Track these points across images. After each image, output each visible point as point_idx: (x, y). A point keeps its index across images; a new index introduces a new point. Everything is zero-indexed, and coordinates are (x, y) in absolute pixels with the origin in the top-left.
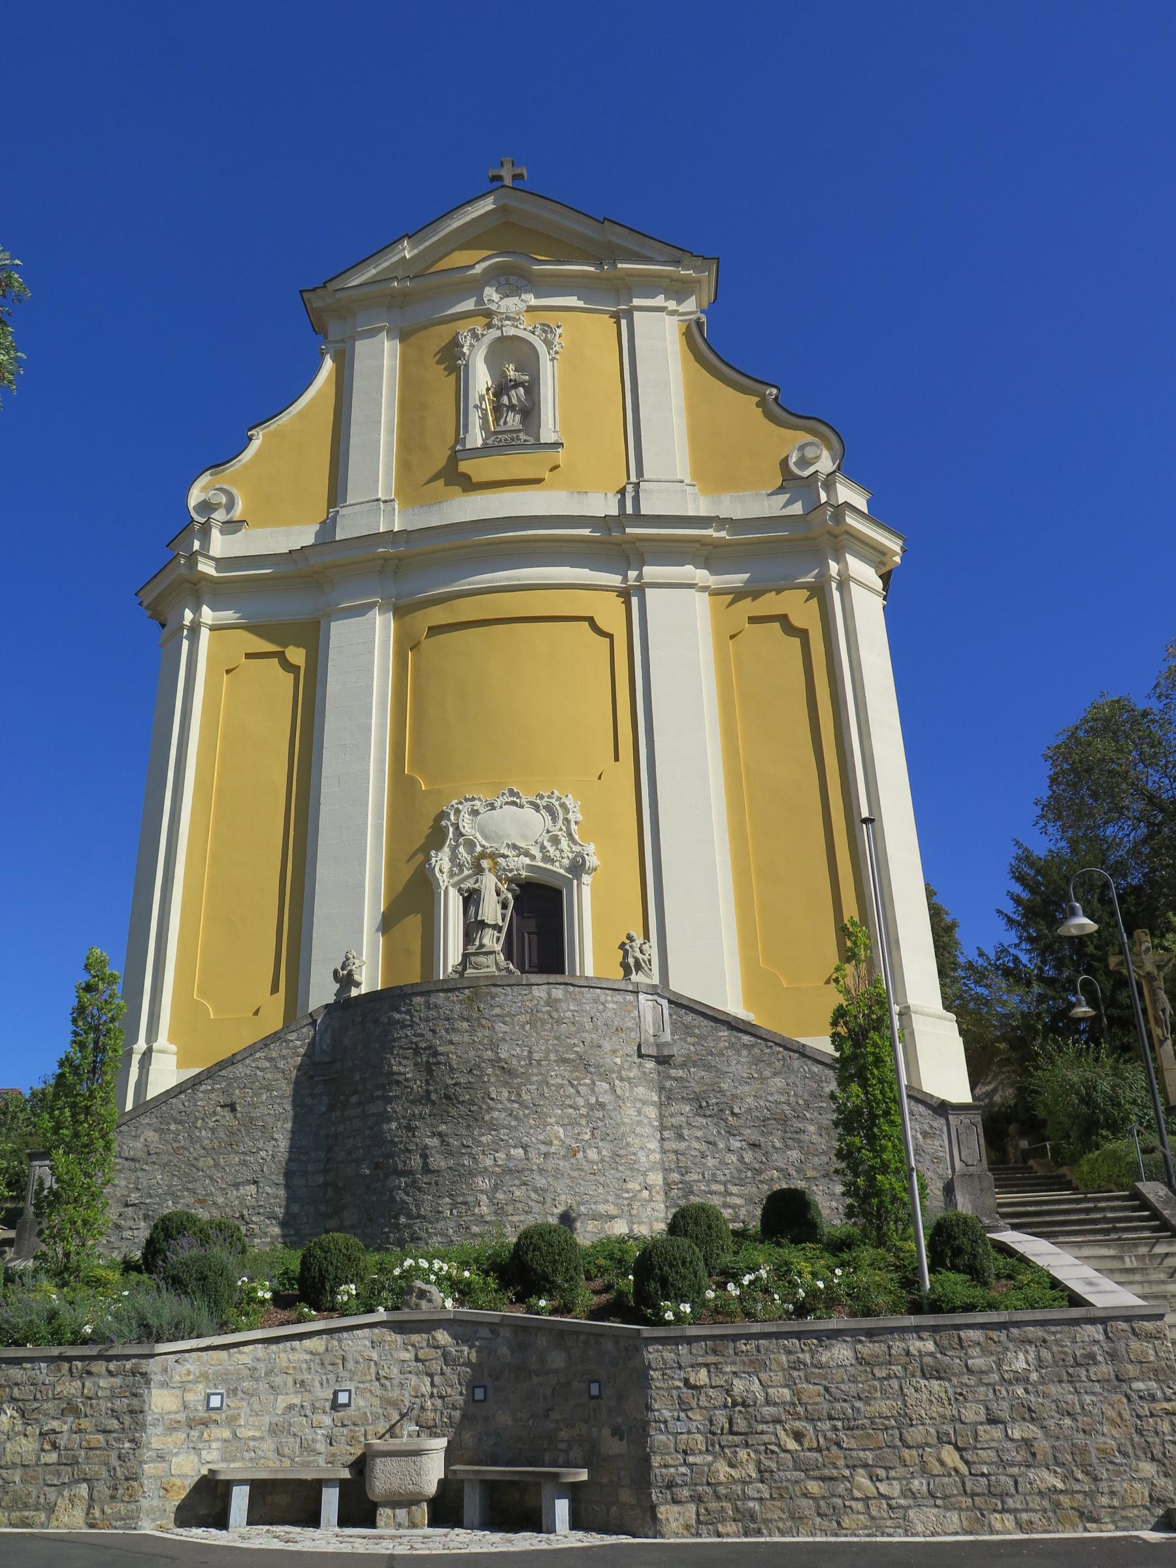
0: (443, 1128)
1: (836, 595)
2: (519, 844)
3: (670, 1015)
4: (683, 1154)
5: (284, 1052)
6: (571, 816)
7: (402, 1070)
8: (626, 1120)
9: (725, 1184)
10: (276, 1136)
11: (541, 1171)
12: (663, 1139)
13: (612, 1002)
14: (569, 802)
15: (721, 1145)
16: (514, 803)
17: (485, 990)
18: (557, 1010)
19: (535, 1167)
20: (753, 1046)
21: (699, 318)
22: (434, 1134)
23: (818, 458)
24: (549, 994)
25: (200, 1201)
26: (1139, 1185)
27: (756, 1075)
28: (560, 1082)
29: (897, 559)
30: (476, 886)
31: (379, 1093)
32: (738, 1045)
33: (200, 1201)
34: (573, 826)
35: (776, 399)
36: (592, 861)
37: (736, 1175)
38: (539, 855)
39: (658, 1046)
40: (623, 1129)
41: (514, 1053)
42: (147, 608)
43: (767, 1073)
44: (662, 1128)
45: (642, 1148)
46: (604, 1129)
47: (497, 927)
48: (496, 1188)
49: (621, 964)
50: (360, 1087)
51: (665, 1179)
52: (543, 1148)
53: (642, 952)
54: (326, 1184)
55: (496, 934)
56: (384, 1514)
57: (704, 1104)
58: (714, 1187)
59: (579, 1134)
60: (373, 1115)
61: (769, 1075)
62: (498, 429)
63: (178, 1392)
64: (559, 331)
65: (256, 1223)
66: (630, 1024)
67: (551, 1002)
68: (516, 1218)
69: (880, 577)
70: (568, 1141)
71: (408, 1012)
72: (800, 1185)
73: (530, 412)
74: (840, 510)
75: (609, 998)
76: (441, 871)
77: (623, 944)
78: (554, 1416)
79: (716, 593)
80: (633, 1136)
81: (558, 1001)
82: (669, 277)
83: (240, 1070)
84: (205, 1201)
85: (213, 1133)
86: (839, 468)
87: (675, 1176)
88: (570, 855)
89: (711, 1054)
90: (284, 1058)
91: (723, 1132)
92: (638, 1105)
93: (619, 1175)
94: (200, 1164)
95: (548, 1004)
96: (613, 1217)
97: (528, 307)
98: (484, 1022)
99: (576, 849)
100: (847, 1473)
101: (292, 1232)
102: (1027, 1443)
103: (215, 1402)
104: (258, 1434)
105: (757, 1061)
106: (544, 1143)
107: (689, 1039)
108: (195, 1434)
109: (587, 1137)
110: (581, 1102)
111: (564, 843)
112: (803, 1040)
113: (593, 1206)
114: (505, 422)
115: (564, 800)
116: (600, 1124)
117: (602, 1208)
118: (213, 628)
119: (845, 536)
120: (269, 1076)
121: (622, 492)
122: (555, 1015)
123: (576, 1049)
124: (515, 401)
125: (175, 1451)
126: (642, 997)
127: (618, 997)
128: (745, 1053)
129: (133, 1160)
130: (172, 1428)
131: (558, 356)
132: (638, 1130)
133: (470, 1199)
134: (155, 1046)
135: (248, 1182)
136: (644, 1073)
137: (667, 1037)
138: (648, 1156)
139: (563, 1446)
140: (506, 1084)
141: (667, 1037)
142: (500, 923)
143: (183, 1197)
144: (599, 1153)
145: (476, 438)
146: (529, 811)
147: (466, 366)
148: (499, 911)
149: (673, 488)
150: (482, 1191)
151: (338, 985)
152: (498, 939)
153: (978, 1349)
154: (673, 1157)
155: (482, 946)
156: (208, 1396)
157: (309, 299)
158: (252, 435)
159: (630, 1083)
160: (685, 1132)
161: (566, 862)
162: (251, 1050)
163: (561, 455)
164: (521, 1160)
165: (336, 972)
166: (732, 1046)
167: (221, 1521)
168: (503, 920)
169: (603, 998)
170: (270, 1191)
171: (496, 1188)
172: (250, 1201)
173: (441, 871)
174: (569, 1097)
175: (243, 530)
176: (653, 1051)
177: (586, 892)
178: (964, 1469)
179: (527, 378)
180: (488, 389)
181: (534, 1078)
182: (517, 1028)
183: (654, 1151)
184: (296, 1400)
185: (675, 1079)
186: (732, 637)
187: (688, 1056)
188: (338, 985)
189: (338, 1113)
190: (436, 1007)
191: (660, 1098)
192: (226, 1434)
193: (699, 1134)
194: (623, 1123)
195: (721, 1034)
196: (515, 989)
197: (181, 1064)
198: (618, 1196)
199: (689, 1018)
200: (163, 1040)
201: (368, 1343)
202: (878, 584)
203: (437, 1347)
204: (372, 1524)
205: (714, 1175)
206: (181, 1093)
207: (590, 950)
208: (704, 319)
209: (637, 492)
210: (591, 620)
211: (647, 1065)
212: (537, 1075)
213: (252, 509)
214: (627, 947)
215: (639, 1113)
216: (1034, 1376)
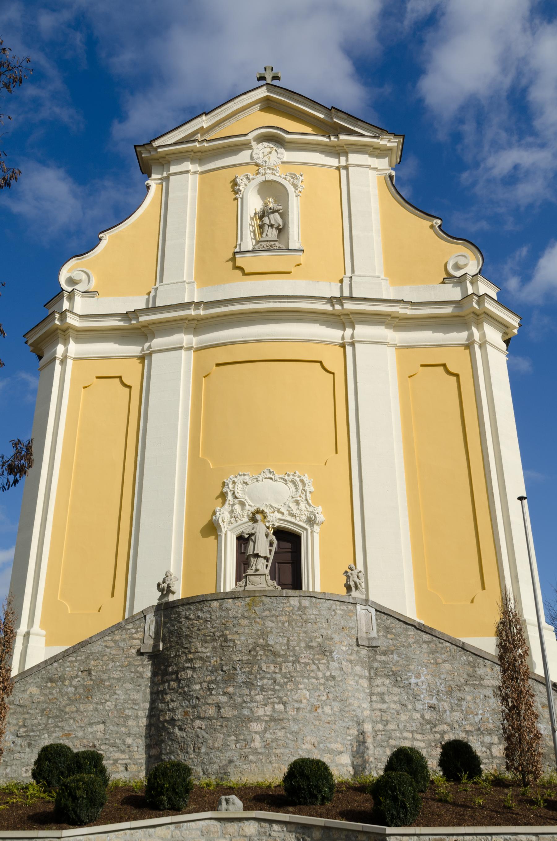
0: (231, 690)
2: (274, 505)
3: (377, 619)
4: (385, 712)
5: (124, 636)
6: (307, 488)
7: (204, 650)
8: (350, 688)
9: (412, 732)
10: (118, 692)
11: (294, 719)
12: (371, 701)
13: (340, 609)
14: (306, 479)
15: (410, 707)
16: (271, 478)
17: (258, 599)
18: (305, 614)
19: (291, 718)
20: (430, 642)
21: (391, 173)
22: (224, 694)
23: (466, 265)
25: (66, 735)
27: (432, 661)
28: (307, 661)
29: (516, 331)
30: (253, 532)
31: (188, 665)
32: (420, 641)
33: (66, 735)
34: (309, 495)
35: (440, 227)
36: (321, 517)
37: (420, 727)
38: (286, 513)
39: (369, 639)
40: (347, 694)
41: (277, 641)
42: (30, 345)
44: (372, 694)
45: (359, 707)
46: (335, 694)
47: (267, 559)
48: (266, 730)
49: (345, 586)
51: (373, 728)
52: (296, 705)
53: (358, 577)
57: (399, 679)
58: (406, 734)
59: (319, 696)
62: (262, 239)
64: (301, 178)
65: (103, 750)
66: (352, 624)
67: (302, 608)
68: (278, 751)
69: (504, 341)
70: (312, 700)
71: (209, 612)
72: (462, 736)
73: (282, 230)
74: (481, 298)
75: (338, 607)
76: (223, 520)
77: (346, 572)
79: (399, 348)
80: (353, 698)
81: (306, 608)
82: (372, 146)
84: (70, 735)
85: (76, 689)
86: (480, 272)
87: (380, 726)
88: (306, 513)
89: (403, 646)
90: (124, 640)
91: (411, 698)
92: (356, 678)
93: (344, 724)
94: (67, 709)
95: (299, 609)
96: (341, 752)
97: (282, 162)
98: (258, 620)
99: (311, 509)
101: (127, 757)
105: (433, 652)
106: (297, 701)
107: (389, 636)
109: (324, 698)
110: (320, 675)
111: (303, 505)
112: (463, 639)
113: (328, 745)
114: (267, 235)
115: (303, 477)
116: (333, 690)
117: (334, 746)
118: (75, 359)
119: (483, 315)
120: (114, 652)
121: (341, 281)
122: (304, 617)
123: (317, 640)
124: (273, 222)
126: (359, 607)
127: (344, 607)
128: (425, 646)
129: (21, 706)
131: (300, 194)
132: (357, 695)
133: (248, 737)
134: (32, 631)
135: (99, 723)
136: (360, 657)
137: (374, 634)
138: (362, 712)
140: (274, 662)
141: (374, 634)
142: (269, 556)
143: (54, 732)
144: (332, 709)
145: (249, 244)
146: (280, 484)
147: (242, 198)
148: (268, 548)
149: (373, 280)
150: (256, 733)
151: (160, 593)
152: (267, 566)
154: (378, 713)
155: (257, 570)
157: (140, 151)
158: (102, 237)
159: (351, 663)
160: (387, 698)
161: (304, 518)
162: (102, 635)
163: (302, 258)
164: (282, 713)
165: (159, 585)
166: (416, 642)
168: (270, 554)
170: (113, 729)
171: (266, 730)
172: (99, 735)
173: (223, 520)
174: (312, 671)
175: (96, 298)
176: (365, 643)
177: (316, 537)
179: (280, 207)
180: (256, 214)
181: (291, 659)
182: (280, 625)
183: (366, 709)
185: (380, 662)
186: (410, 377)
187: (388, 647)
188: (160, 593)
189: (160, 678)
190: (227, 610)
191: (370, 674)
193: (396, 699)
194: (347, 690)
195: (409, 633)
196: (279, 598)
197: (48, 644)
199: (389, 622)
200: (36, 628)
201: (199, 833)
202: (504, 346)
203: (246, 836)
205: (405, 726)
208: (393, 173)
209: (351, 281)
210: (321, 362)
211: (362, 652)
212: (292, 656)
213: (98, 283)
214: (349, 574)
215: (357, 682)
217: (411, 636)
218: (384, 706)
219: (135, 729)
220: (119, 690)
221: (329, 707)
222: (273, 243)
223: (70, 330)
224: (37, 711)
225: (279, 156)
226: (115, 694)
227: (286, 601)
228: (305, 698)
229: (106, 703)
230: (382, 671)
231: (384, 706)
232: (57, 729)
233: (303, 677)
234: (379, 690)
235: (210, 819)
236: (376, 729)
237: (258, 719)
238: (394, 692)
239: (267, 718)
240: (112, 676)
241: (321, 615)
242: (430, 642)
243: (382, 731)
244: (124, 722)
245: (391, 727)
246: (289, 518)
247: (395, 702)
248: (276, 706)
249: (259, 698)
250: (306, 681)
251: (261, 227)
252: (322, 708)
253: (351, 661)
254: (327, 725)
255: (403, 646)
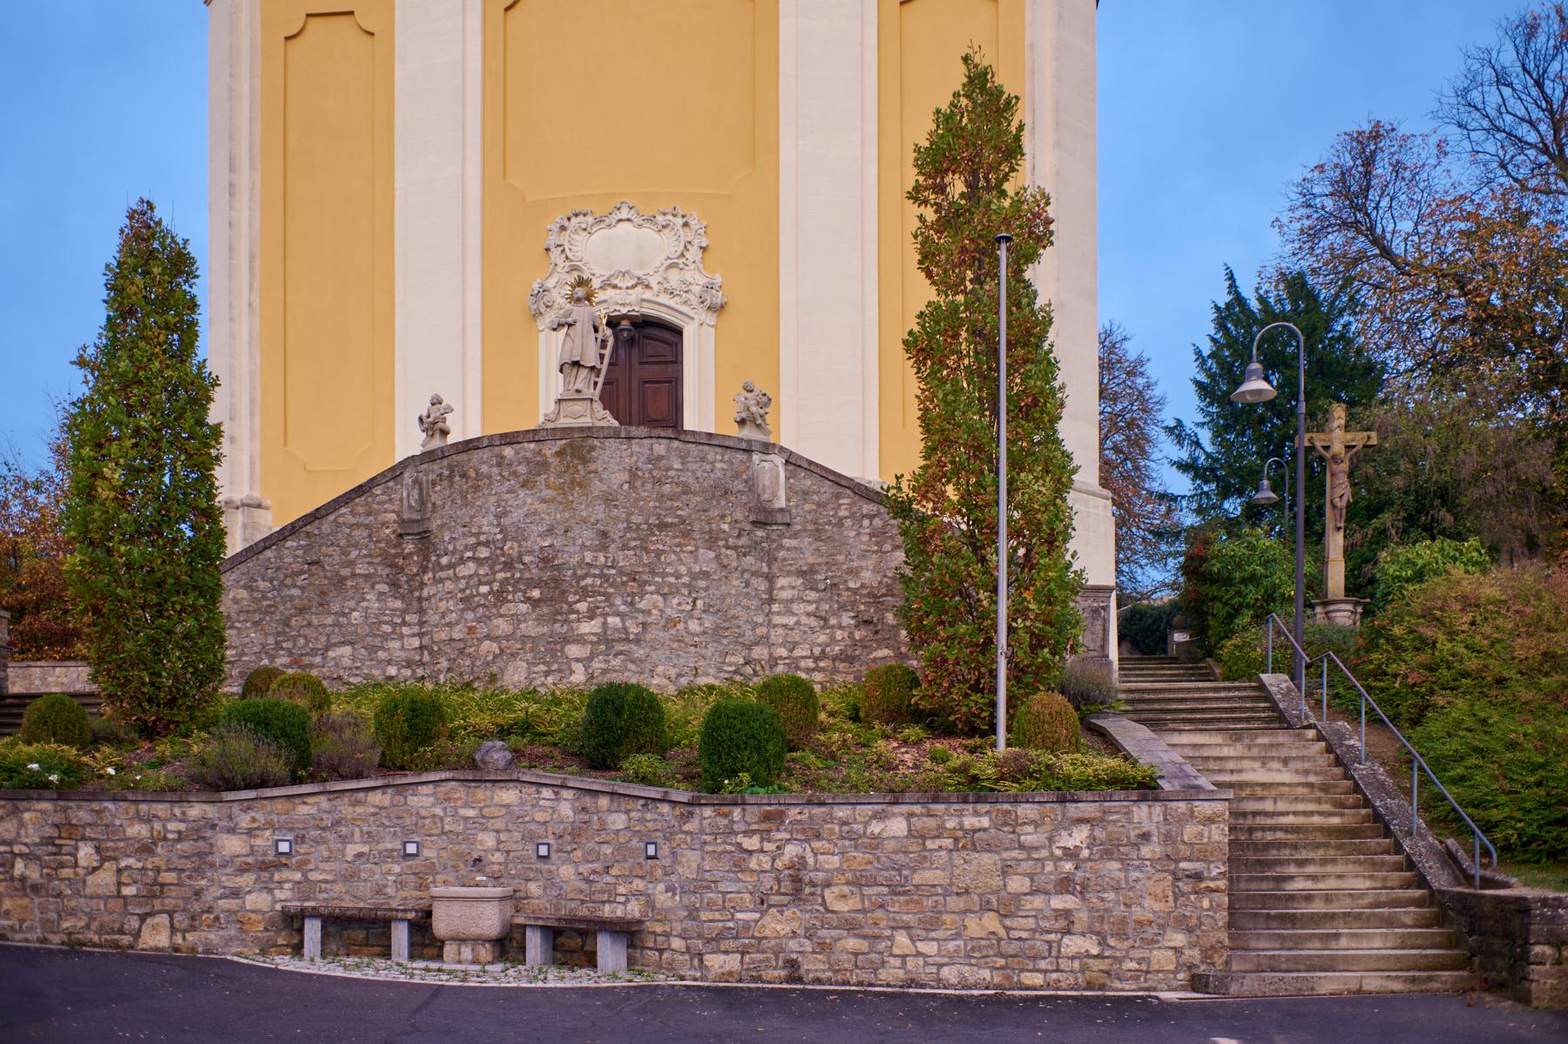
15: (833, 621)
26: (1263, 676)
31: (470, 554)
43: (887, 547)
48: (591, 658)
50: (451, 548)
54: (421, 648)
56: (449, 949)
63: (245, 837)
78: (614, 872)
83: (326, 526)
100: (888, 932)
102: (1066, 914)
103: (284, 847)
104: (329, 877)
110: (683, 569)
128: (866, 522)
135: (343, 643)
139: (622, 899)
152: (596, 384)
156: (277, 842)
167: (298, 950)
169: (710, 457)
172: (346, 662)
178: (1002, 933)
184: (365, 849)
192: (298, 876)
198: (720, 670)
204: (439, 957)
207: (703, 406)
215: (747, 584)
216: (1085, 853)
218: (791, 621)
219: (399, 653)
228: (656, 607)
231: (791, 621)
233: (653, 573)
234: (785, 595)
235: (453, 780)
237: (580, 640)
239: (595, 639)
242: (874, 516)
245: (798, 652)
246: (664, 299)
247: (809, 615)
248: (610, 620)
253: (735, 548)
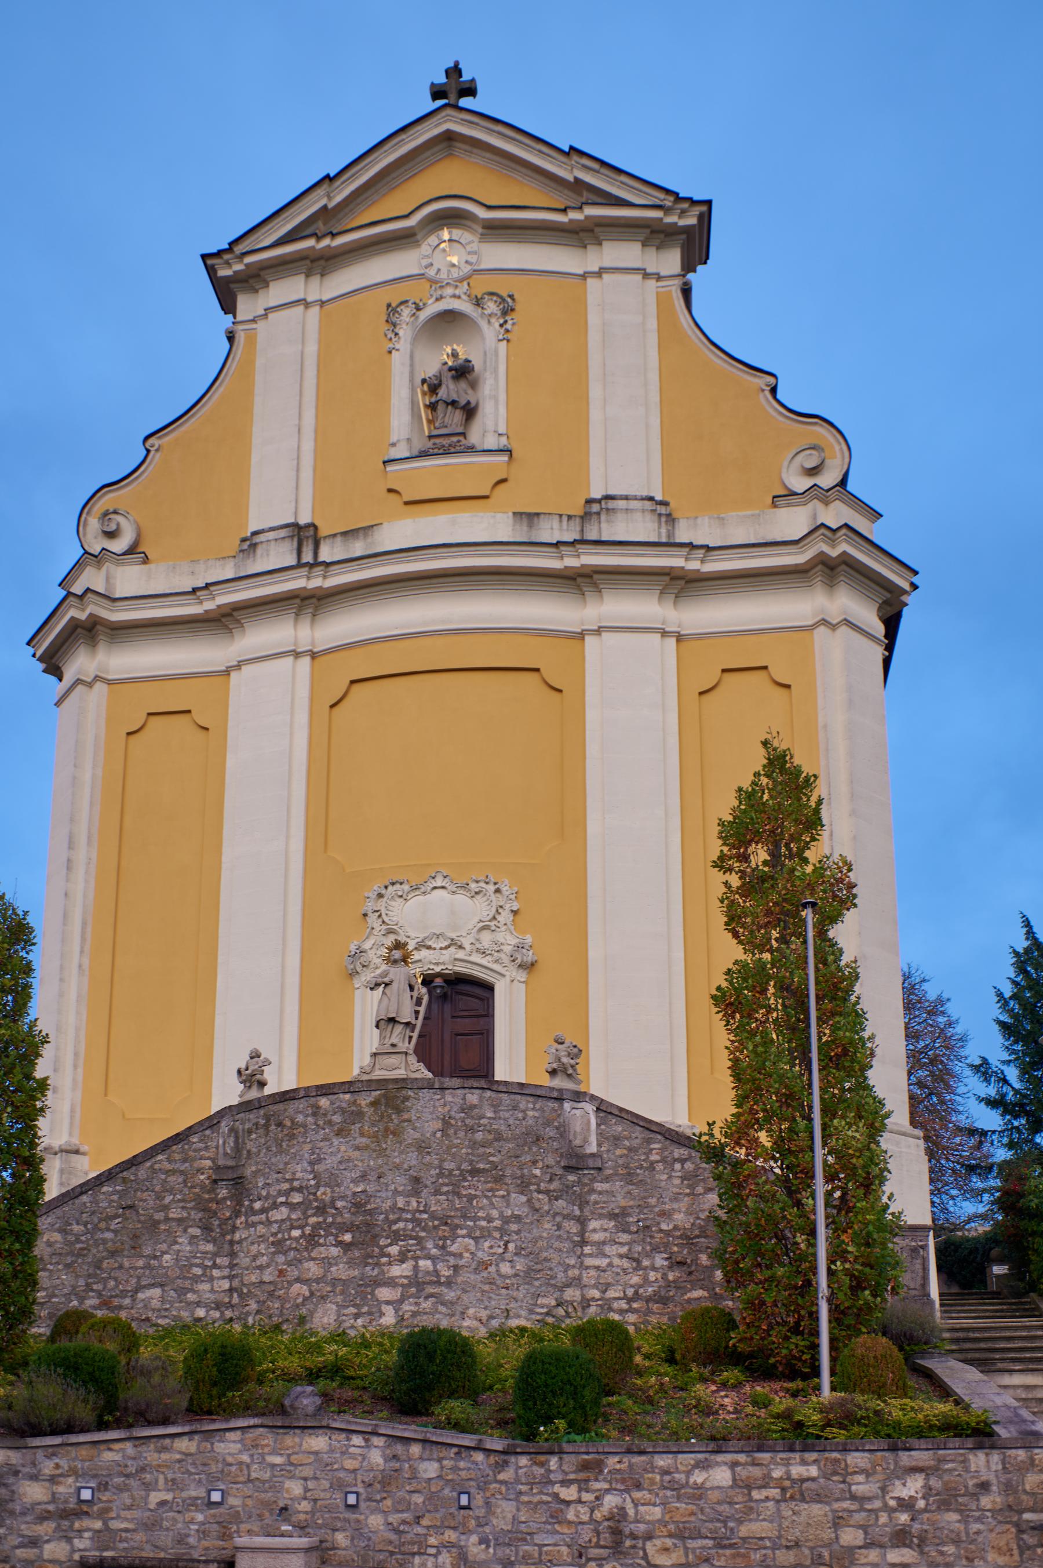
1: (749, 513)
15: (646, 1263)
24: (464, 1099)
28: (473, 1192)
43: (700, 1189)
48: (401, 1301)
54: (231, 1290)
55: (408, 1033)
59: (491, 1247)
60: (276, 1222)
61: (702, 1191)
63: (47, 1484)
75: (531, 1106)
78: (425, 1522)
103: (86, 1495)
104: (130, 1526)
108: (66, 1523)
110: (495, 1213)
123: (491, 1159)
125: (46, 1538)
130: (44, 1517)
139: (433, 1551)
142: (413, 1022)
153: (863, 1476)
156: (79, 1489)
160: (607, 1249)
168: (417, 1018)
169: (522, 1106)
172: (155, 1303)
184: (169, 1497)
192: (98, 1525)
195: (652, 1146)
206: (82, 1193)
215: (559, 1227)
216: (921, 1504)
217: (654, 1152)
218: (603, 1262)
220: (181, 1237)
221: (508, 1264)
222: (455, 439)
223: (99, 627)
224: (60, 1267)
225: (469, 248)
226: (176, 1243)
227: (439, 1097)
228: (467, 1250)
229: (161, 1256)
230: (603, 1208)
231: (603, 1262)
232: (91, 1294)
233: (465, 1217)
236: (589, 1296)
237: (391, 1283)
238: (621, 1240)
239: (406, 1281)
240: (171, 1215)
241: (500, 1118)
242: (686, 1160)
243: (598, 1300)
244: (192, 1284)
245: (611, 1294)
246: (476, 958)
247: (621, 1256)
249: (394, 1250)
250: (471, 1223)
251: (432, 407)
252: (497, 1265)
253: (547, 1192)
254: (504, 1291)
255: (641, 1167)
